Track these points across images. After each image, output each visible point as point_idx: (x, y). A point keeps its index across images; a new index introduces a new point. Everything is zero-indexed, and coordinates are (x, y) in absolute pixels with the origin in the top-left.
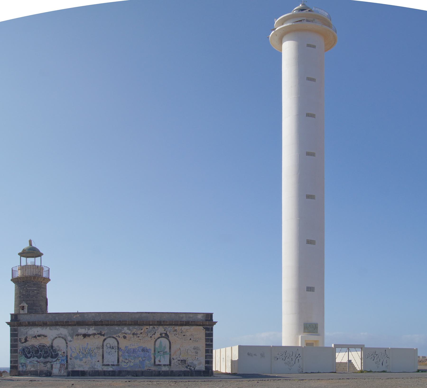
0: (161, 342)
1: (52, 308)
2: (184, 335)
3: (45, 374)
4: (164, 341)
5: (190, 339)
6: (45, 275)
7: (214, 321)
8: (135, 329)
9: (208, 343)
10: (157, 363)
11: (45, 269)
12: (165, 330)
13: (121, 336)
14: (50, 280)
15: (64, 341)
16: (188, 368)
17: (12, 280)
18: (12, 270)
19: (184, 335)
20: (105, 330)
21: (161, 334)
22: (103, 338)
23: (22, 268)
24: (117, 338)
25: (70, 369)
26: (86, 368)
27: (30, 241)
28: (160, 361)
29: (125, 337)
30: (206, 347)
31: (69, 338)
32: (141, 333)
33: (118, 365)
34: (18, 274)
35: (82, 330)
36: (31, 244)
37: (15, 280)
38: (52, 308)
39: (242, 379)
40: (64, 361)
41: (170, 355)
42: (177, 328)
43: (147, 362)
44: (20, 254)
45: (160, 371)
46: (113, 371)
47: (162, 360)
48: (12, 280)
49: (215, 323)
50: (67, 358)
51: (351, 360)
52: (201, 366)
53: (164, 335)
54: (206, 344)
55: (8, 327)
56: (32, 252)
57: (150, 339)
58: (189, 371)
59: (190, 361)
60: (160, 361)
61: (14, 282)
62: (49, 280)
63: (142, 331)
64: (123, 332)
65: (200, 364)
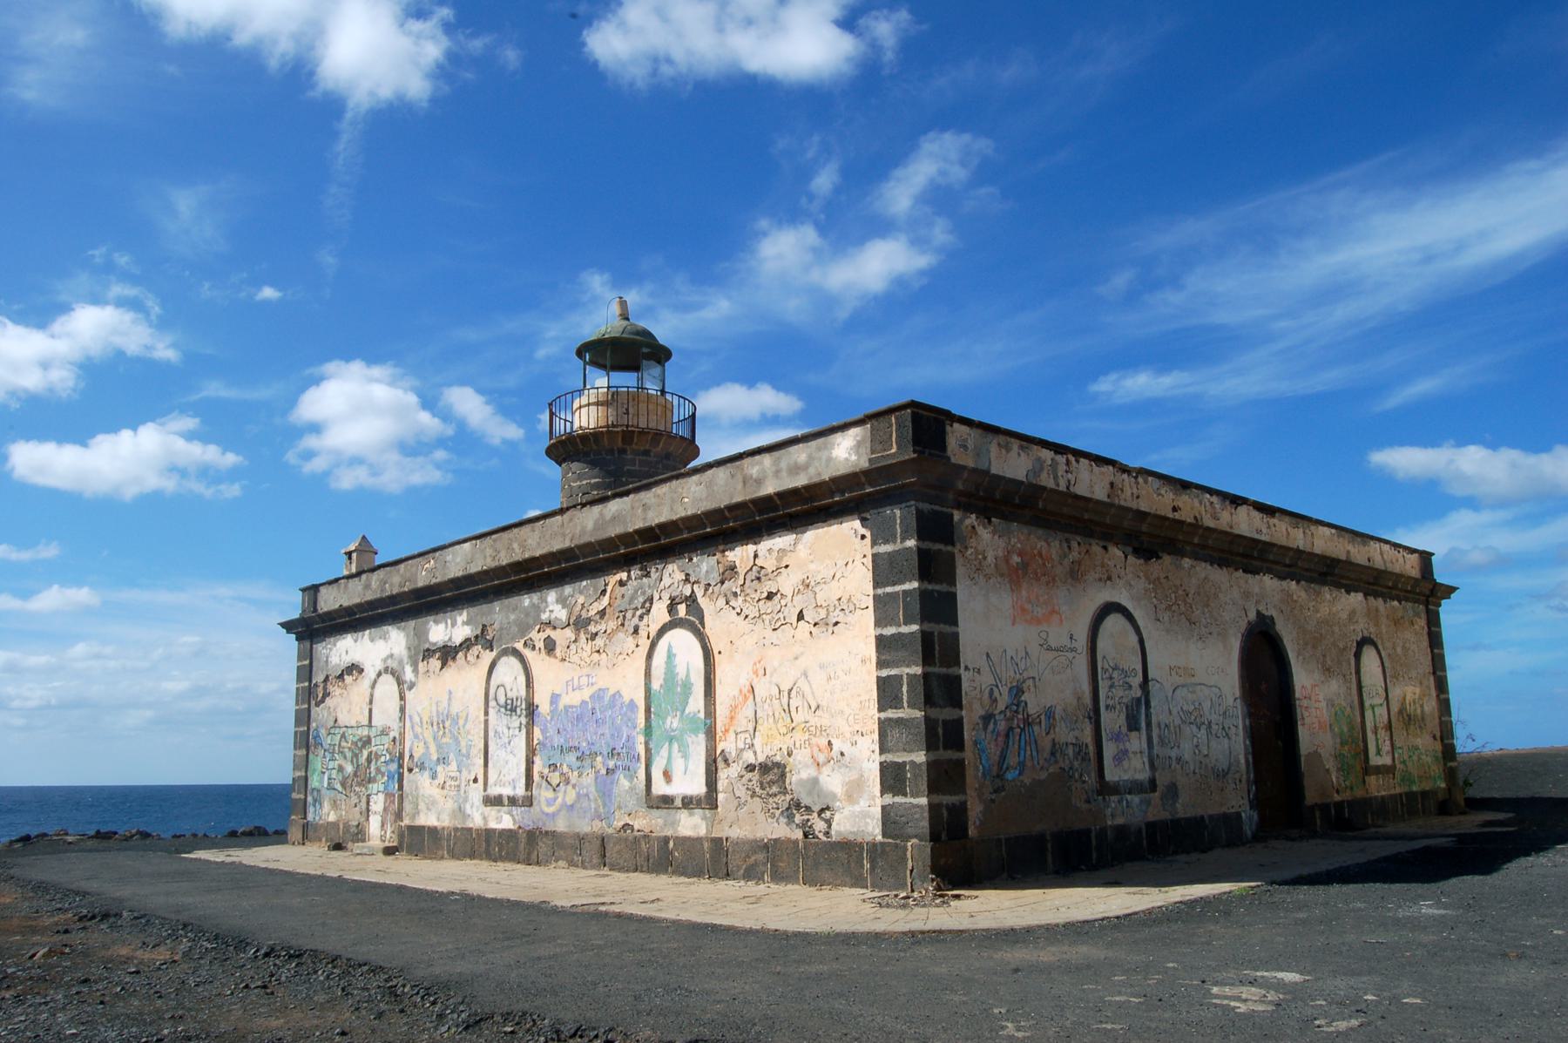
0: (670, 656)
2: (770, 596)
3: (562, 846)
4: (682, 643)
5: (800, 617)
8: (580, 594)
9: (889, 631)
10: (660, 788)
12: (687, 580)
13: (538, 638)
15: (395, 687)
16: (798, 819)
19: (770, 596)
20: (499, 613)
21: (672, 608)
22: (488, 656)
24: (527, 653)
25: (406, 822)
28: (667, 776)
29: (550, 647)
30: (881, 664)
31: (409, 674)
32: (602, 613)
33: (528, 801)
35: (440, 631)
39: (599, 900)
40: (1107, 707)
41: (711, 734)
42: (740, 555)
43: (624, 783)
45: (666, 840)
46: (508, 835)
47: (678, 766)
50: (401, 766)
51: (98, 832)
52: (863, 804)
53: (682, 610)
54: (881, 642)
57: (630, 642)
58: (796, 842)
59: (804, 775)
60: (667, 776)
63: (605, 601)
64: (544, 617)
65: (854, 789)
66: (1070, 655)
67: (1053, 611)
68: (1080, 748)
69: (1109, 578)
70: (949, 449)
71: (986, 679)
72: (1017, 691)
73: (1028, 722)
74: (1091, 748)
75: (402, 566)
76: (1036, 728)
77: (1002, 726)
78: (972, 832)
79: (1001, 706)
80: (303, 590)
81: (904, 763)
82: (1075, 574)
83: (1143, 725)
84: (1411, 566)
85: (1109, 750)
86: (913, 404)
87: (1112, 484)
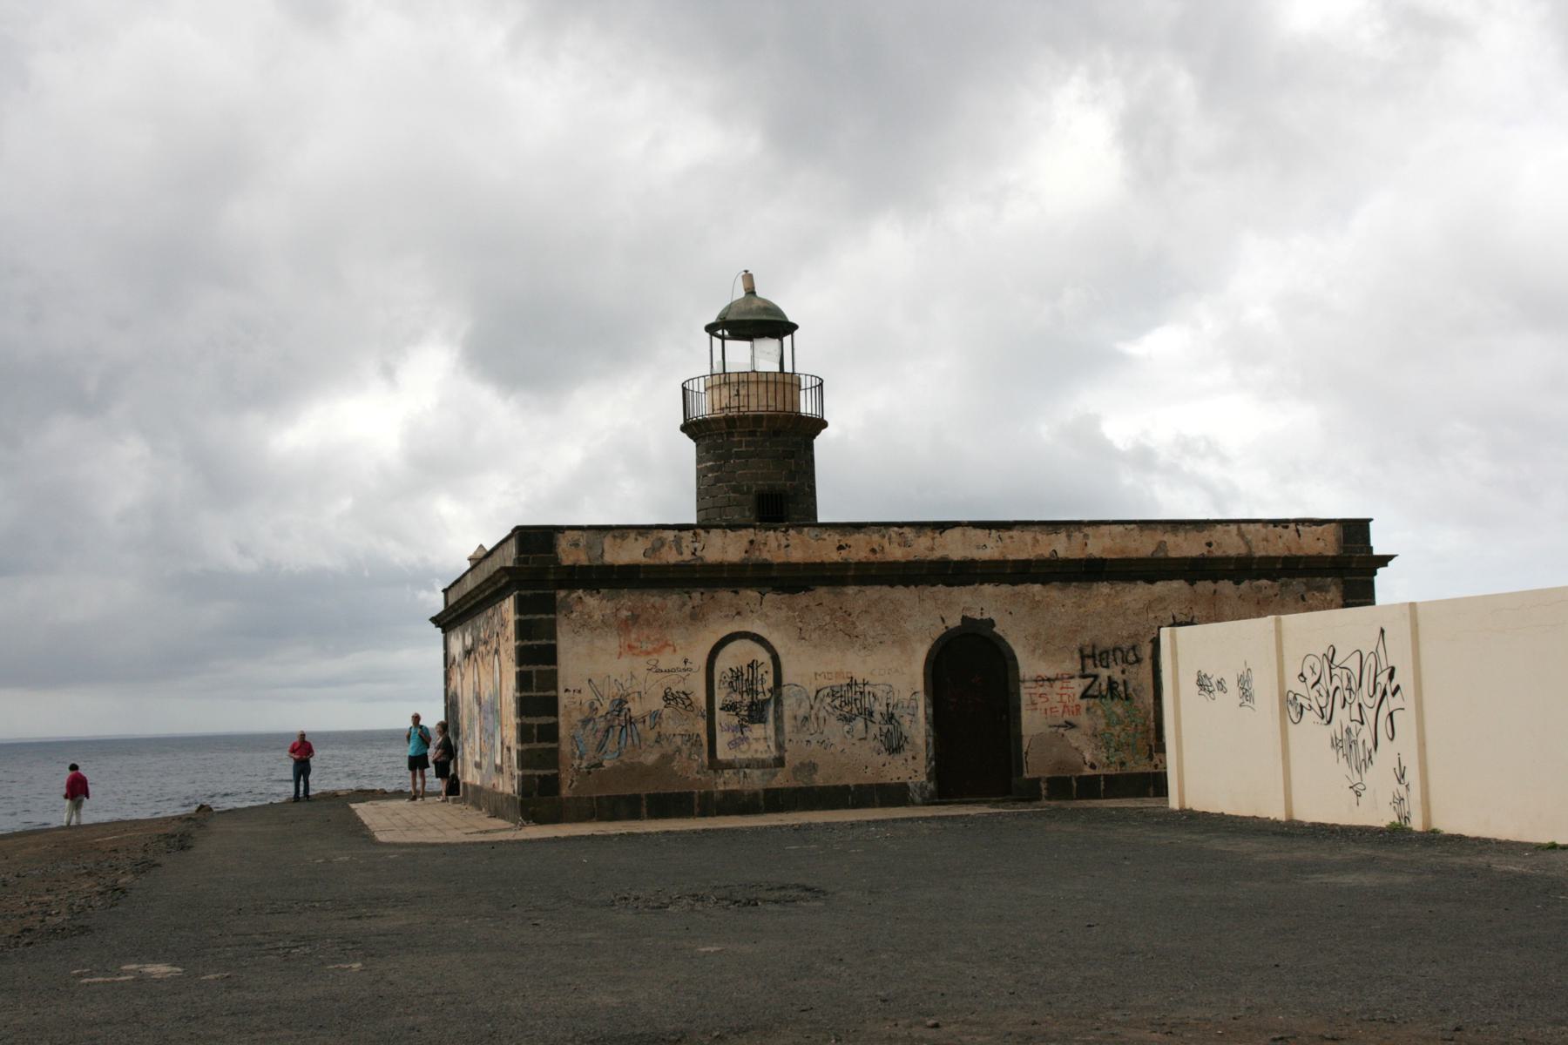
1: (821, 519)
6: (806, 407)
7: (1376, 552)
11: (806, 382)
14: (824, 424)
17: (684, 429)
18: (684, 389)
23: (723, 380)
26: (390, 788)
27: (748, 278)
34: (703, 408)
36: (751, 292)
37: (691, 428)
38: (821, 519)
44: (711, 329)
48: (684, 429)
49: (1384, 560)
55: (1378, 549)
56: (758, 322)
61: (691, 436)
62: (820, 424)
66: (684, 674)
67: (667, 645)
68: (692, 739)
69: (739, 613)
70: (559, 550)
71: (588, 695)
72: (621, 703)
73: (630, 721)
74: (704, 738)
75: (1015, 533)
76: (640, 726)
77: (602, 725)
78: (565, 792)
79: (602, 712)
80: (1356, 530)
81: (1080, 797)
82: (696, 617)
83: (771, 718)
84: (1326, 545)
85: (722, 739)
86: (518, 528)
87: (752, 542)
